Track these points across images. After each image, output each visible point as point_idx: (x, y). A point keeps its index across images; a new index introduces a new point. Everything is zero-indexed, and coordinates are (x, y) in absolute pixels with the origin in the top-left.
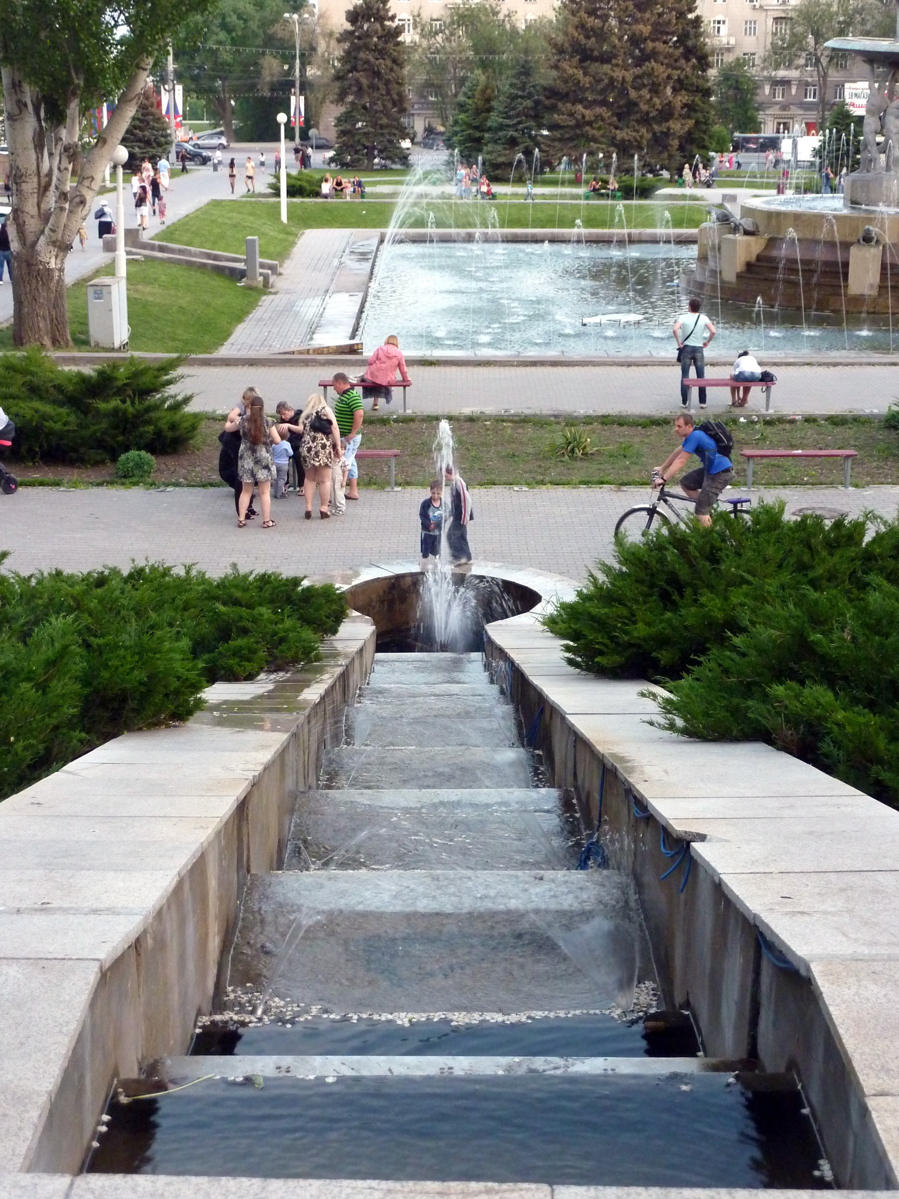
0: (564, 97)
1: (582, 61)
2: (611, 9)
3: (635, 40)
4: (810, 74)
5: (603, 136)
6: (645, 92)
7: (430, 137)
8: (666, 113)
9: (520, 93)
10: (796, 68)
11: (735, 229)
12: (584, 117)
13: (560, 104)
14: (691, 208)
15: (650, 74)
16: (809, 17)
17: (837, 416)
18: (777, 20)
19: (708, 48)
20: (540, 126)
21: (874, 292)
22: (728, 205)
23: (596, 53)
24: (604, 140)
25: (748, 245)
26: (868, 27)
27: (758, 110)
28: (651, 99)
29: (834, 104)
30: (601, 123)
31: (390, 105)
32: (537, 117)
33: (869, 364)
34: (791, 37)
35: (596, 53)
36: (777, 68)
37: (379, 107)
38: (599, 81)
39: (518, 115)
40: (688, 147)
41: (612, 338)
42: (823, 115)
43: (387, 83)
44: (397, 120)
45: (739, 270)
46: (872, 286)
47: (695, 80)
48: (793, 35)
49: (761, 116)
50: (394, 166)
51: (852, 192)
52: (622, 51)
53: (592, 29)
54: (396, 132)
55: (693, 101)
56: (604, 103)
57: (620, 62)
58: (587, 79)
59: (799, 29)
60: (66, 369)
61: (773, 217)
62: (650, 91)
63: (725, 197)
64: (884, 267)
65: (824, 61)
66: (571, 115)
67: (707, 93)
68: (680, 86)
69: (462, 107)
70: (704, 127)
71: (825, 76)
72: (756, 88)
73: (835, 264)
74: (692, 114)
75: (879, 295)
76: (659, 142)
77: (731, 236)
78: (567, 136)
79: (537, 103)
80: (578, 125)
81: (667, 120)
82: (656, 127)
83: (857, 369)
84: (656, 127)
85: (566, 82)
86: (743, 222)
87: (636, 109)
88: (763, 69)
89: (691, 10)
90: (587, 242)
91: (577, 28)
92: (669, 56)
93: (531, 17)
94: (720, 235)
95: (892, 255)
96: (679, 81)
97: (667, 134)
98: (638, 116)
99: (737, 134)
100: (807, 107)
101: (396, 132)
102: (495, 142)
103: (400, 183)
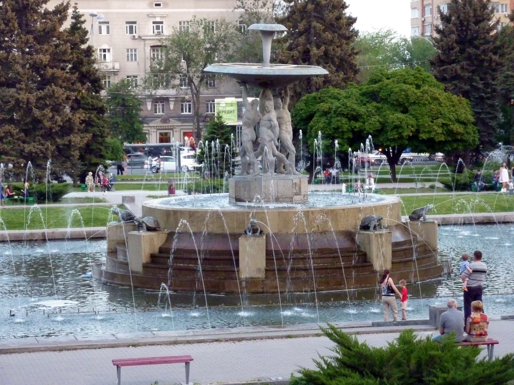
2: (13, 41)
3: (36, 67)
4: (185, 92)
5: (12, 149)
6: (47, 111)
8: (67, 129)
10: (173, 88)
11: (139, 226)
14: (97, 210)
15: (51, 96)
16: (181, 45)
19: (99, 74)
21: (261, 275)
22: (127, 205)
25: (152, 239)
26: (230, 52)
27: (142, 123)
28: (53, 117)
29: (206, 116)
30: (10, 138)
34: (166, 62)
36: (156, 88)
40: (88, 156)
42: (198, 125)
45: (144, 262)
46: (259, 270)
47: (90, 100)
48: (168, 59)
49: (145, 128)
51: (236, 192)
52: (26, 77)
55: (89, 118)
56: (11, 121)
57: (23, 86)
59: (173, 55)
62: (52, 110)
63: (124, 198)
64: (269, 253)
65: (196, 81)
67: (101, 110)
68: (77, 105)
72: (139, 105)
73: (229, 252)
74: (90, 128)
75: (266, 277)
76: (62, 154)
77: (135, 233)
81: (68, 134)
82: (58, 140)
83: (258, 343)
84: (58, 140)
86: (145, 220)
87: (40, 126)
88: (144, 88)
89: (83, 42)
90: (12, 241)
94: (126, 232)
95: (275, 243)
96: (76, 101)
97: (69, 146)
98: (42, 132)
99: (126, 144)
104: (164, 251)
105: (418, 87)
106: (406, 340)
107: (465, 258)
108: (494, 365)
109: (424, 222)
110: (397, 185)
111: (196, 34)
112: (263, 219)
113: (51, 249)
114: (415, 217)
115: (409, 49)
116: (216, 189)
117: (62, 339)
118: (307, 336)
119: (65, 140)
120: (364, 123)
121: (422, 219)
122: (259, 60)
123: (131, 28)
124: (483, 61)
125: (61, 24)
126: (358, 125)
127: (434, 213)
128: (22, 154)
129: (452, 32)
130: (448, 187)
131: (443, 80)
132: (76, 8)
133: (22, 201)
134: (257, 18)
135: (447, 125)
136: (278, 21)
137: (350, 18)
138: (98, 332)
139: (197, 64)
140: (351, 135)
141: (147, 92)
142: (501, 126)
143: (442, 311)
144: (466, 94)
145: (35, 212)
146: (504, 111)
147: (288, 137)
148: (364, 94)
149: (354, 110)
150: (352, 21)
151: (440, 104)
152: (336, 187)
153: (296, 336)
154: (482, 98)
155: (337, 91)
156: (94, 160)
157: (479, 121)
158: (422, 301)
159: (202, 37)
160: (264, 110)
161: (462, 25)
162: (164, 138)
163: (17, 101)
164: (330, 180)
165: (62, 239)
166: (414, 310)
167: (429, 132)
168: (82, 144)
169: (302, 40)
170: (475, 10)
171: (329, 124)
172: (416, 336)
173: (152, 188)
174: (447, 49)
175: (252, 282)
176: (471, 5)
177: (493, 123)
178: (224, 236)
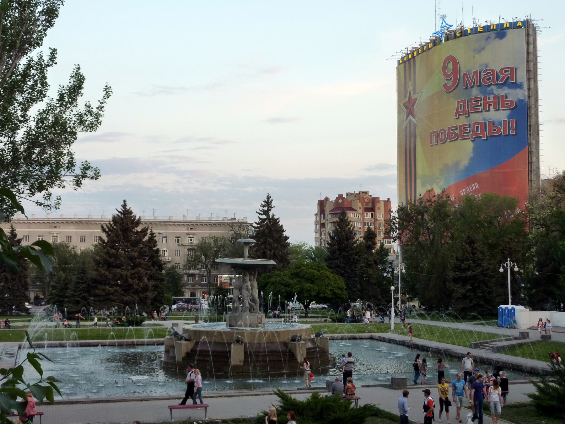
0: (101, 283)
1: (108, 267)
2: (120, 245)
3: (131, 259)
7: (37, 302)
9: (81, 281)
11: (181, 338)
12: (109, 291)
13: (99, 286)
14: (159, 330)
15: (138, 273)
17: (236, 419)
18: (188, 250)
20: (90, 296)
21: (242, 364)
22: (174, 328)
23: (114, 264)
24: (118, 301)
26: (226, 252)
27: (182, 287)
29: (214, 284)
31: (21, 287)
32: (88, 292)
33: (246, 395)
35: (114, 264)
36: (189, 269)
37: (16, 287)
38: (116, 276)
39: (80, 291)
41: (95, 393)
43: (20, 277)
44: (24, 293)
46: (240, 361)
48: (196, 255)
49: (183, 289)
50: (22, 314)
51: (230, 321)
53: (113, 254)
54: (23, 298)
58: (111, 275)
59: (198, 253)
60: (261, 381)
61: (198, 333)
62: (138, 280)
63: (173, 324)
64: (246, 353)
65: (209, 266)
66: (104, 290)
68: (151, 278)
69: (54, 287)
70: (161, 295)
71: (210, 272)
76: (142, 302)
77: (179, 341)
78: (102, 299)
79: (89, 285)
80: (107, 295)
81: (146, 292)
82: (141, 295)
83: (241, 398)
84: (141, 295)
85: (101, 276)
86: (184, 335)
88: (184, 270)
91: (106, 254)
92: (146, 265)
93: (83, 249)
97: (146, 298)
98: (133, 290)
99: (173, 297)
100: (203, 285)
101: (23, 298)
102: (70, 302)
103: (29, 321)
104: (193, 351)
105: (319, 271)
106: (315, 397)
107: (344, 356)
108: (359, 410)
109: (323, 338)
110: (309, 320)
111: (210, 244)
112: (243, 336)
113: (139, 350)
114: (318, 335)
115: (314, 252)
116: (220, 321)
117: (143, 395)
118: (265, 395)
119: (144, 295)
120: (292, 288)
121: (321, 336)
122: (241, 256)
123: (178, 240)
124: (350, 258)
125: (144, 237)
126: (289, 289)
127: (327, 334)
128: (122, 301)
129: (335, 245)
130: (334, 321)
131: (331, 268)
132: (151, 230)
133: (122, 325)
134: (239, 236)
135: (333, 290)
136: (251, 237)
137: (286, 237)
138: (159, 392)
139: (210, 258)
140: (285, 294)
141: (185, 272)
142: (359, 291)
143: (332, 382)
144: (342, 275)
145: (131, 330)
146: (360, 283)
147: (256, 295)
148: (292, 274)
149: (288, 282)
150: (287, 238)
151: (329, 279)
152: (279, 320)
153: (259, 395)
154: (350, 277)
155: (279, 272)
156: (158, 305)
157: (348, 288)
158: (322, 378)
159: (213, 245)
160: (244, 281)
161: (340, 241)
162: (193, 294)
163: (121, 275)
164: (275, 316)
165: (142, 344)
166: (319, 382)
167: (324, 293)
168: (152, 297)
169: (262, 247)
170: (346, 234)
171: (275, 289)
172: (320, 395)
173: (187, 319)
174: (333, 253)
175: (236, 367)
176: (344, 231)
177: (355, 289)
178: (223, 344)
